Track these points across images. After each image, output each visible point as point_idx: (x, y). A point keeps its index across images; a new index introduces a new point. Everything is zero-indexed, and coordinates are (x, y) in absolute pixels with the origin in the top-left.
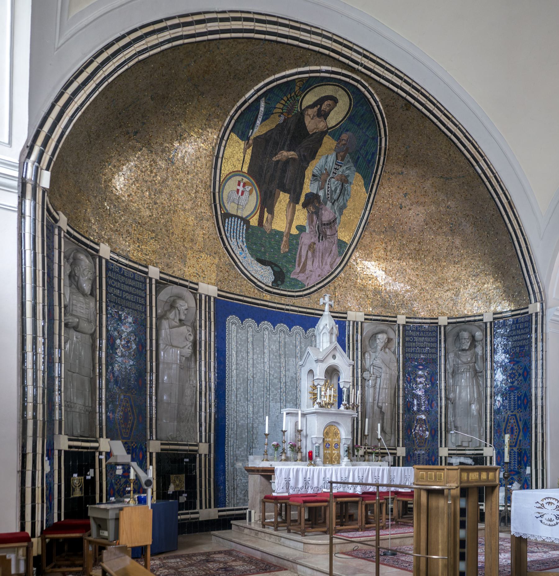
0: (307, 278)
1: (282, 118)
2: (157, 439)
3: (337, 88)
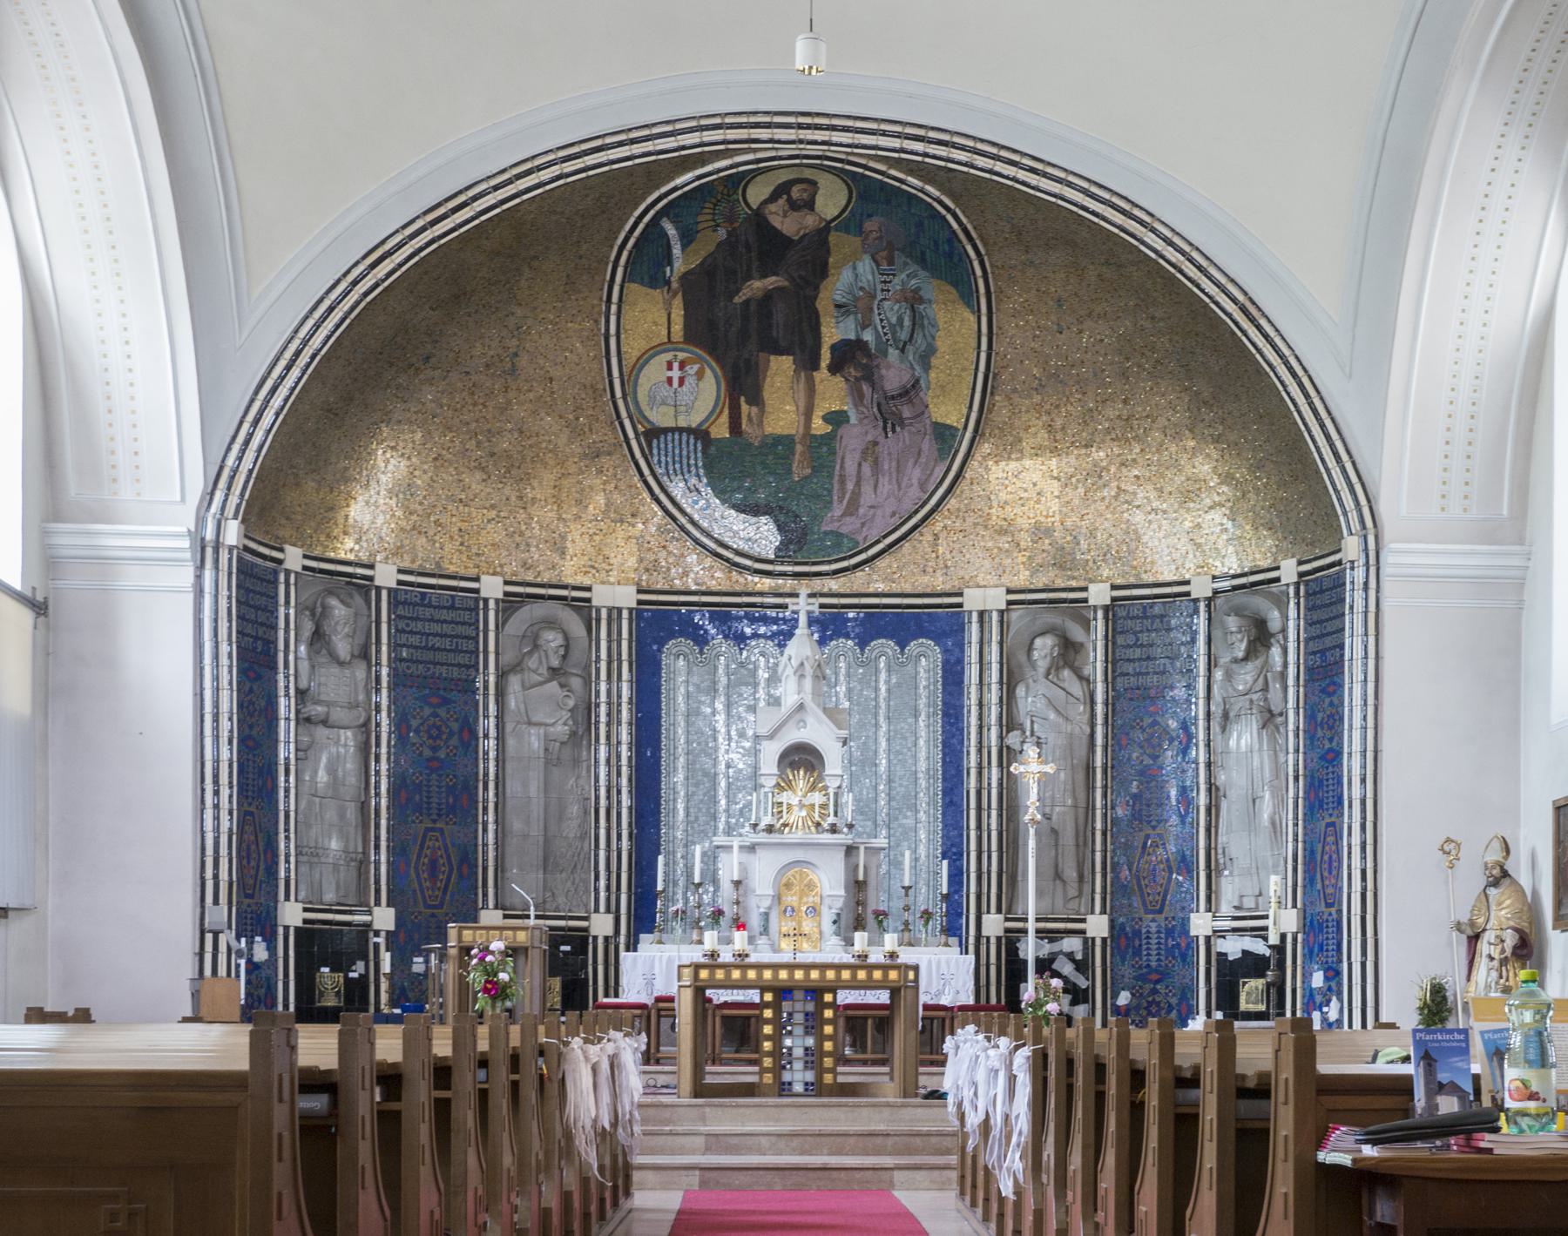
0: (863, 524)
2: (496, 908)
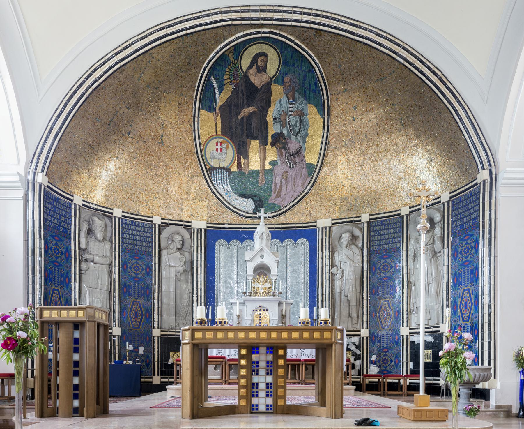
0: (282, 200)
1: (233, 85)
2: (158, 328)
3: (259, 44)
